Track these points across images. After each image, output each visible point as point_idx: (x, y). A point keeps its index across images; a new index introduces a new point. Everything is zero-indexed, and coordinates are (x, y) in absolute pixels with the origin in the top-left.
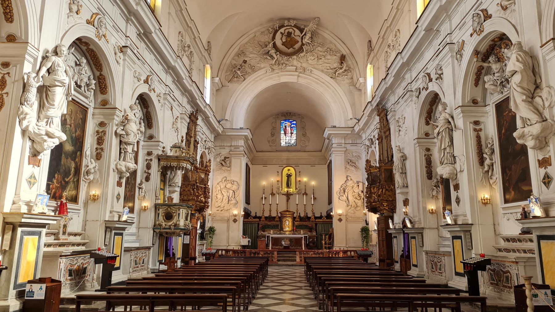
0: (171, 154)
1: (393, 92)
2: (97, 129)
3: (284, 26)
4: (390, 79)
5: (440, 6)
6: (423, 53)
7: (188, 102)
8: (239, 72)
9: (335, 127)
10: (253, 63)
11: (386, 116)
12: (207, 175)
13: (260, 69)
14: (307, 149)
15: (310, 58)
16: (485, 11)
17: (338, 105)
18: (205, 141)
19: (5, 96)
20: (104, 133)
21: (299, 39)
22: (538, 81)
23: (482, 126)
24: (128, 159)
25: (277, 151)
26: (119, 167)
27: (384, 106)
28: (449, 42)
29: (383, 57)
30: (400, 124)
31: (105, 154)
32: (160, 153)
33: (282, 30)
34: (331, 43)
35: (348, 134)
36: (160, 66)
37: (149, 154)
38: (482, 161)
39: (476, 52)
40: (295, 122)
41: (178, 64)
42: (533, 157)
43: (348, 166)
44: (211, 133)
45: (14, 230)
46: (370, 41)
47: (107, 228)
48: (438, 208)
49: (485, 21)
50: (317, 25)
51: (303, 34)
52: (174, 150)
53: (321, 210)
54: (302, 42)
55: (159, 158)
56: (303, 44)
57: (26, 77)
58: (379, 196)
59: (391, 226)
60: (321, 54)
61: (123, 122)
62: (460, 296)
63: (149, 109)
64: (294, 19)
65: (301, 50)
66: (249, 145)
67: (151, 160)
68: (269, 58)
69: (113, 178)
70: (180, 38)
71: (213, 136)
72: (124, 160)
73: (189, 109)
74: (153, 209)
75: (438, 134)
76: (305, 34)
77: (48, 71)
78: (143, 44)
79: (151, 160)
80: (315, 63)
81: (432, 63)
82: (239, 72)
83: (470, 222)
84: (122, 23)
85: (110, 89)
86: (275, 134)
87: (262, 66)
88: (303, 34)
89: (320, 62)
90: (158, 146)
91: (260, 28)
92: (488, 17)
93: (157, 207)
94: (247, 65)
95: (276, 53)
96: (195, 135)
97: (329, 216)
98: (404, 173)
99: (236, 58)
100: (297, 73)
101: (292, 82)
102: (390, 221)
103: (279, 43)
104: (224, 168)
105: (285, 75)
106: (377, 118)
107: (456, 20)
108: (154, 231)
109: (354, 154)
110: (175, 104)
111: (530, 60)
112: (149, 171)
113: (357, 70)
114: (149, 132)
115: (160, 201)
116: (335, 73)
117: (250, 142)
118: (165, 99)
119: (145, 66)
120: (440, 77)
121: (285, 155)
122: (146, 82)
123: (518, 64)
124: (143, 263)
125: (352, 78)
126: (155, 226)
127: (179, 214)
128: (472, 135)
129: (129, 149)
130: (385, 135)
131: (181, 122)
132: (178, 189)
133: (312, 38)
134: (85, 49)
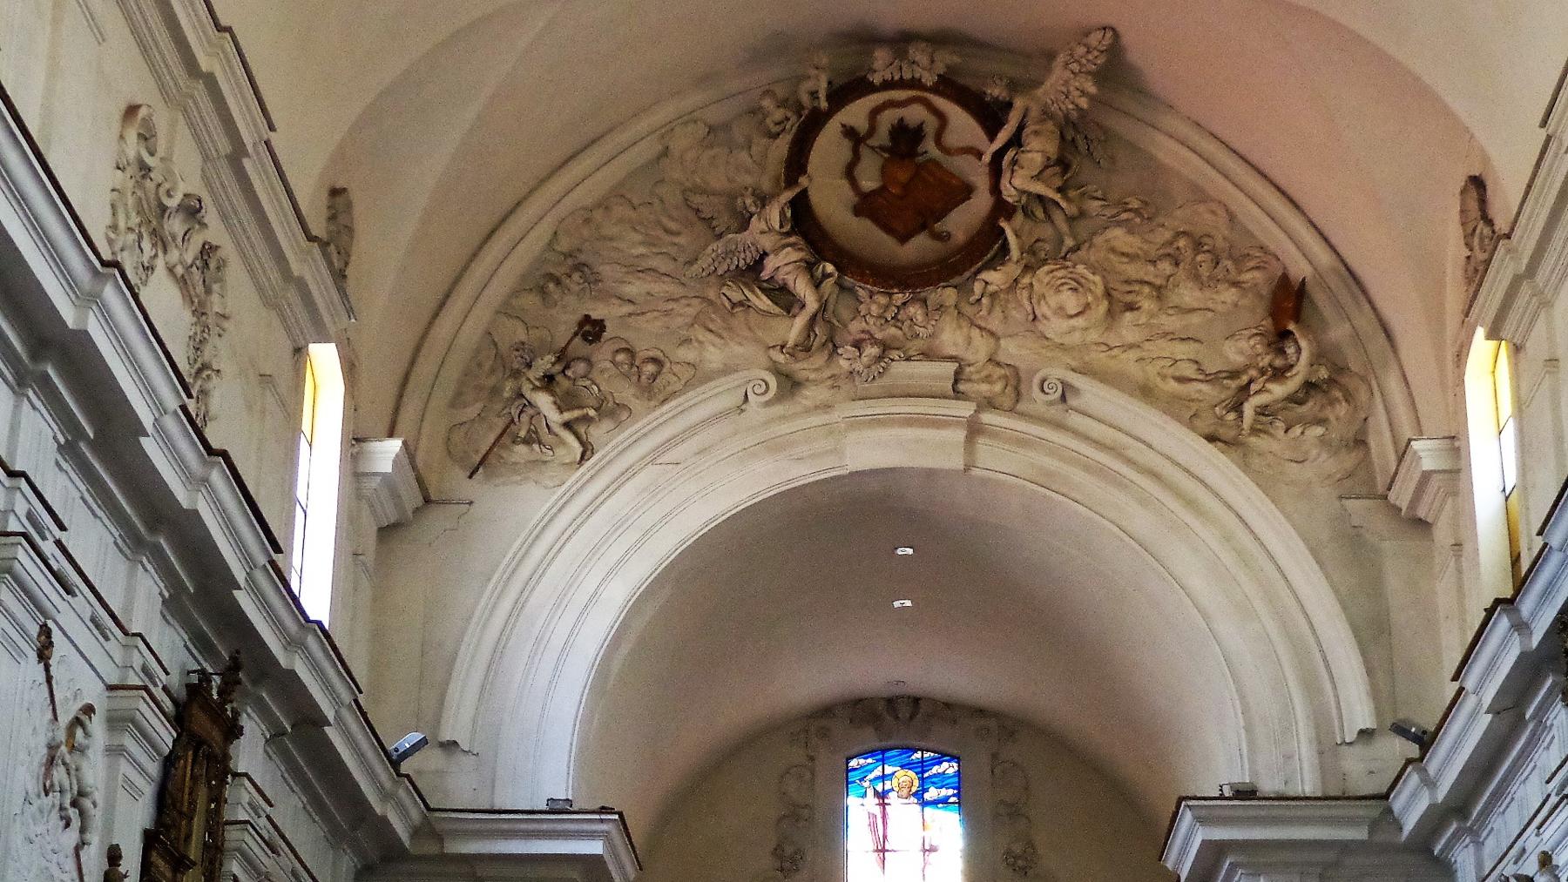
3: (873, 89)
10: (646, 335)
13: (699, 376)
33: (856, 113)
34: (1200, 195)
35: (1345, 847)
40: (949, 768)
46: (1477, 183)
51: (1003, 137)
54: (995, 190)
56: (1002, 208)
60: (1133, 270)
64: (940, 39)
65: (987, 245)
68: (762, 302)
70: (133, 147)
71: (348, 863)
76: (1016, 141)
80: (1094, 336)
82: (544, 401)
87: (714, 355)
88: (1003, 137)
89: (1128, 328)
91: (693, 99)
94: (602, 354)
95: (810, 267)
99: (530, 301)
100: (965, 409)
101: (930, 474)
103: (831, 198)
116: (1237, 408)
119: (283, 860)
125: (1360, 442)
131: (115, 751)
133: (1063, 164)
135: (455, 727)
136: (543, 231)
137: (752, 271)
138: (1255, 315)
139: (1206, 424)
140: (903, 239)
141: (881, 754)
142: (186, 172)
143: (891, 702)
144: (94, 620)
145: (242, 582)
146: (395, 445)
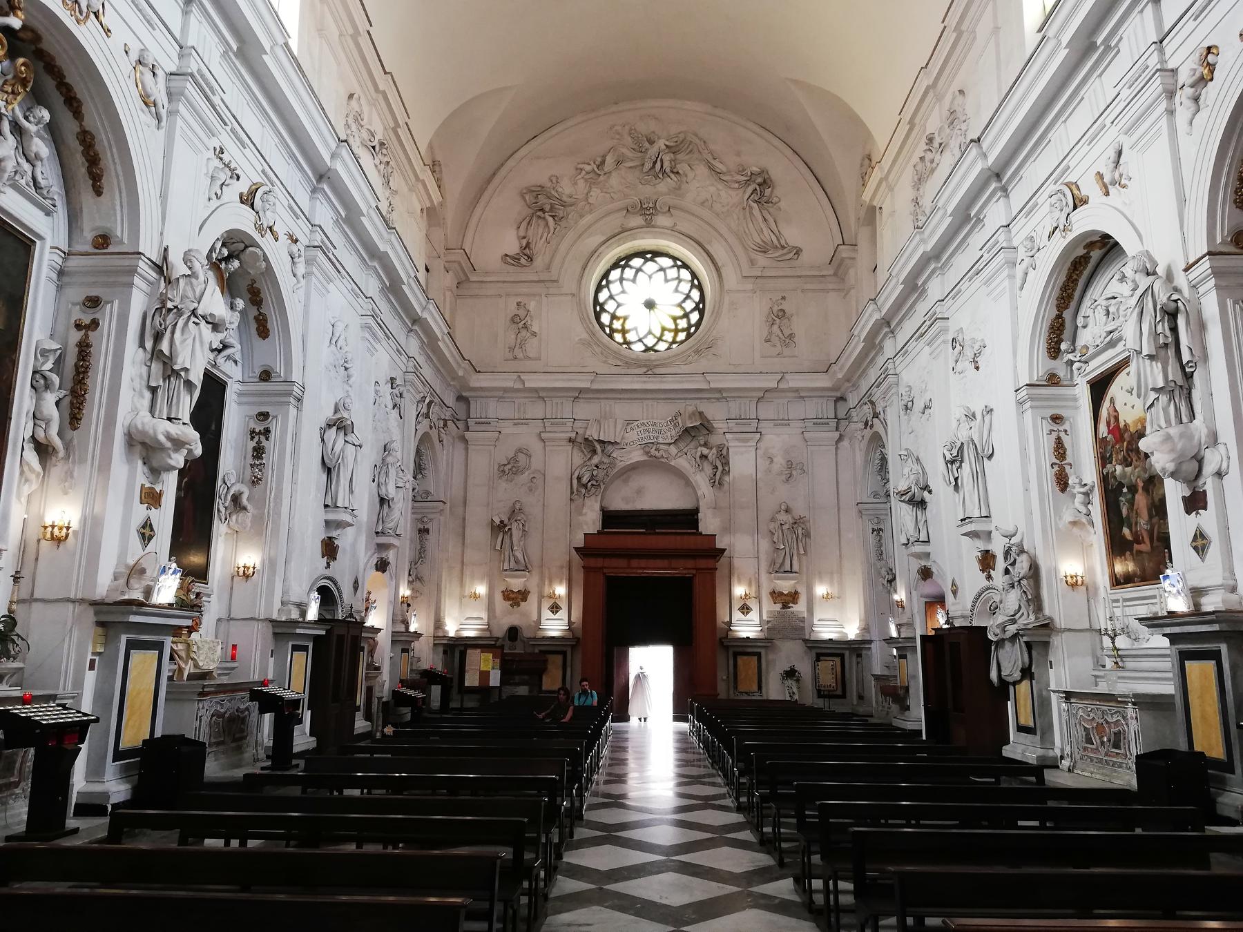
28: (1004, 245)
42: (1174, 493)
48: (1090, 570)
49: (1075, 208)
62: (1207, 833)
81: (1023, 221)
107: (1019, 195)
144: (263, 172)
145: (268, 50)
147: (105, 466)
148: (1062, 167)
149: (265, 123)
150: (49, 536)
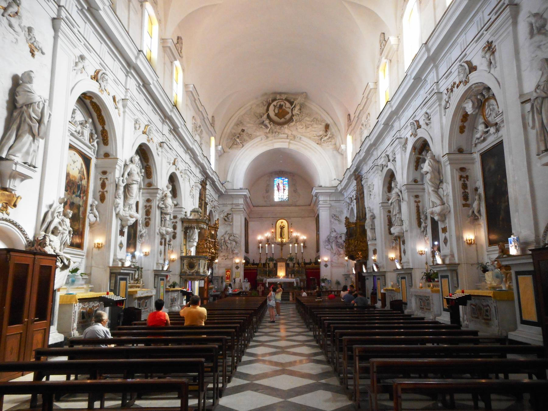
0: (191, 218)
1: (366, 163)
2: (145, 204)
4: (363, 154)
5: (391, 112)
6: (384, 139)
7: (200, 172)
8: (238, 140)
9: (321, 186)
10: (250, 131)
11: (361, 181)
12: (216, 231)
13: (256, 137)
14: (298, 204)
15: (299, 127)
16: (469, 63)
17: (327, 165)
18: (212, 201)
19: (105, 193)
20: (150, 206)
21: (290, 111)
22: (442, 178)
23: (420, 199)
24: (167, 225)
25: (271, 206)
26: (161, 231)
27: (359, 172)
28: (436, 91)
29: (358, 132)
30: (371, 189)
31: (152, 222)
32: (183, 216)
33: (275, 103)
34: (317, 113)
35: (332, 193)
36: (104, 45)
37: (175, 217)
38: (420, 224)
39: (414, 148)
41: (174, 113)
43: (333, 220)
44: (216, 193)
45: (116, 277)
46: (349, 115)
47: (155, 275)
50: (305, 98)
52: (193, 214)
53: (309, 257)
54: (292, 113)
55: (183, 221)
57: (117, 180)
58: (355, 247)
59: (364, 271)
60: (309, 123)
61: (162, 198)
63: (175, 183)
64: (285, 93)
65: (291, 120)
66: (247, 203)
67: (176, 222)
68: (263, 127)
69: (115, 225)
71: (217, 196)
72: (164, 226)
73: (200, 177)
74: (180, 260)
75: (391, 203)
77: (128, 175)
78: (172, 136)
79: (176, 222)
82: (238, 140)
83: (411, 267)
84: (121, 75)
85: (154, 176)
86: (269, 190)
87: (258, 134)
89: (308, 130)
90: (182, 211)
92: (472, 68)
93: (182, 258)
94: (244, 133)
96: (205, 197)
97: (319, 263)
98: (373, 229)
99: (236, 127)
100: (288, 140)
102: (364, 266)
103: (272, 113)
104: (226, 223)
105: (278, 142)
106: (355, 182)
108: (181, 277)
109: (338, 210)
110: (191, 176)
111: (437, 165)
112: (176, 231)
113: (339, 137)
114: (104, 149)
115: (184, 254)
117: (248, 200)
118: (186, 174)
120: (394, 160)
121: (278, 209)
122: (174, 164)
123: (429, 167)
124: (146, 306)
125: (335, 144)
126: (181, 272)
127: (199, 264)
128: (413, 205)
129: (168, 217)
130: (360, 197)
131: (196, 189)
132: (195, 244)
133: (300, 109)
134: (89, 104)
135: (229, 179)
136: (237, 118)
137: (262, 123)
138: (323, 128)
139: (317, 142)
140: (281, 119)
141: (278, 178)
142: (199, 122)
143: (280, 172)
144: (100, 64)
146: (221, 147)
147: (155, 238)
148: (414, 115)
149: (115, 59)
150: (96, 246)
